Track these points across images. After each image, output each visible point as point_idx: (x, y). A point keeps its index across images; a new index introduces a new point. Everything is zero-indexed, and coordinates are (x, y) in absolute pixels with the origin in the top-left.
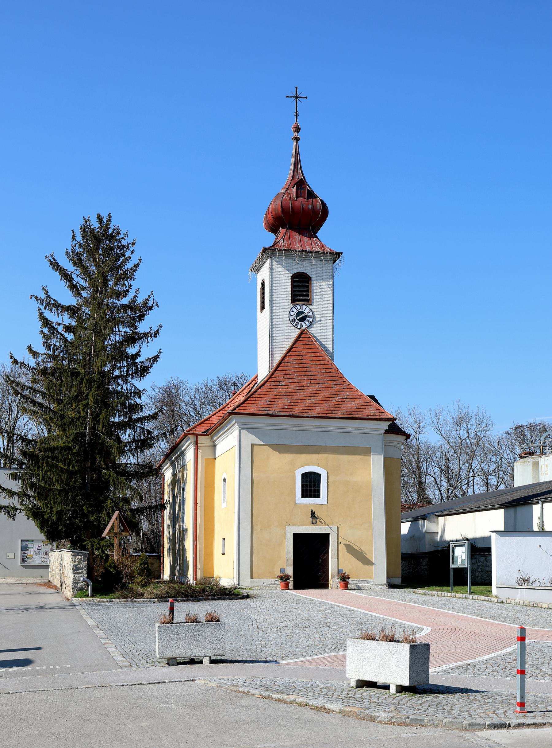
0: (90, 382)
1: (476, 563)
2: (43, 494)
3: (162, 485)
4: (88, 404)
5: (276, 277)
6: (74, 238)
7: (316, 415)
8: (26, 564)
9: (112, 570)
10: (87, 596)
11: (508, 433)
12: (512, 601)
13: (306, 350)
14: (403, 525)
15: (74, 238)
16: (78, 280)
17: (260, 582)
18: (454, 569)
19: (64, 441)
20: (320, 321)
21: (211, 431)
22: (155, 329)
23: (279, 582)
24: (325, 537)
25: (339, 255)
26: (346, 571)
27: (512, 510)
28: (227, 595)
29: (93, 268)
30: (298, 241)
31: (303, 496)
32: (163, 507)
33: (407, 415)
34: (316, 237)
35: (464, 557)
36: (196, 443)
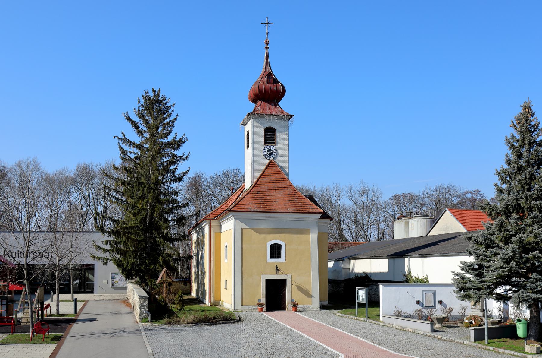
0: (149, 188)
1: (371, 289)
2: (123, 253)
3: (192, 244)
4: (148, 201)
5: (254, 129)
6: (139, 102)
7: (278, 211)
8: (114, 286)
9: (162, 303)
10: (148, 322)
11: (390, 199)
12: (391, 326)
13: (273, 172)
14: (329, 263)
15: (139, 102)
16: (142, 127)
17: (247, 307)
18: (358, 303)
19: (134, 222)
20: (282, 156)
21: (218, 217)
22: (186, 155)
23: (257, 307)
24: (284, 281)
25: (292, 116)
26: (296, 301)
27: (392, 260)
28: (227, 320)
29: (150, 121)
30: (268, 108)
31: (272, 257)
32: (191, 257)
33: (332, 188)
34: (279, 106)
35: (364, 297)
36: (210, 224)
